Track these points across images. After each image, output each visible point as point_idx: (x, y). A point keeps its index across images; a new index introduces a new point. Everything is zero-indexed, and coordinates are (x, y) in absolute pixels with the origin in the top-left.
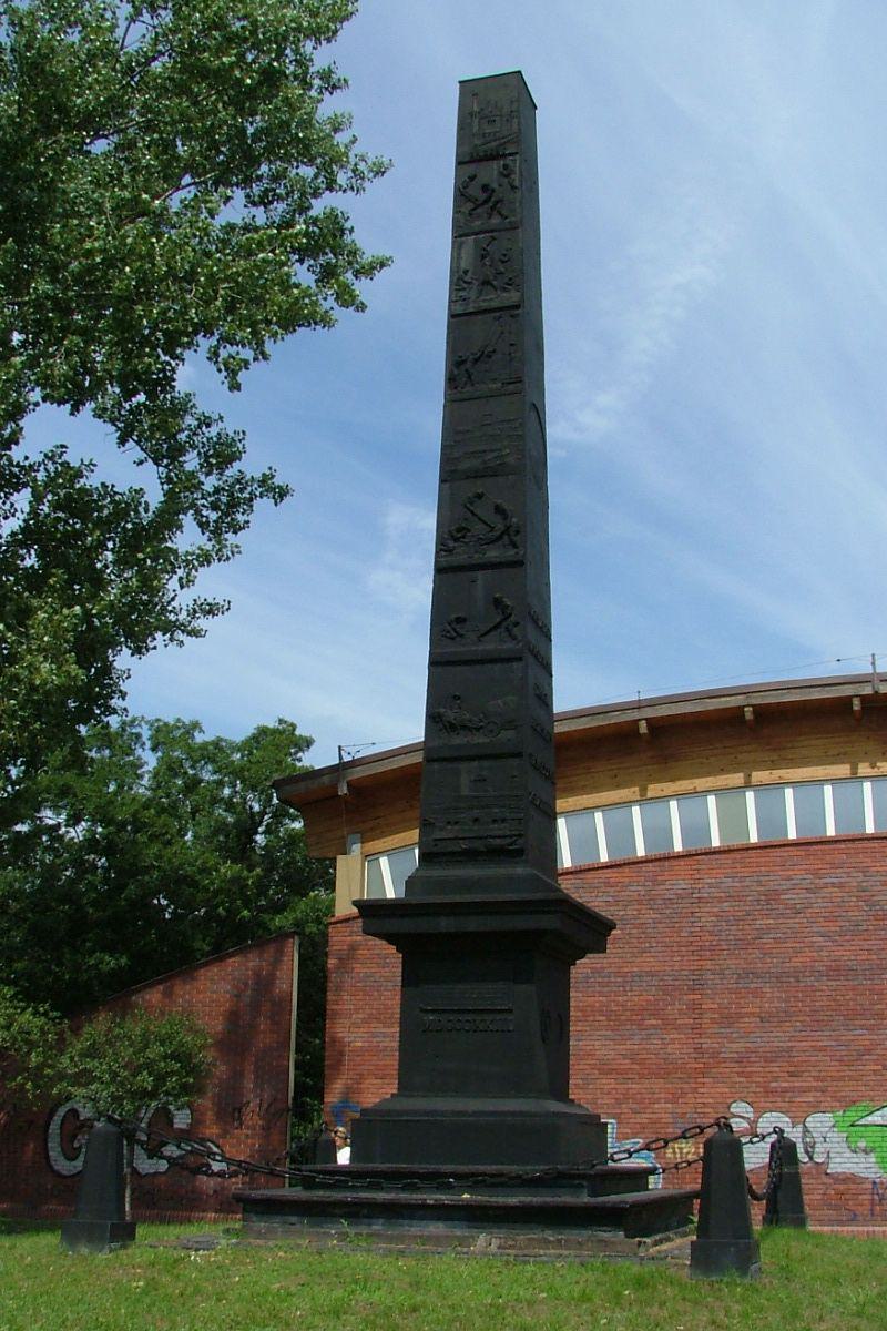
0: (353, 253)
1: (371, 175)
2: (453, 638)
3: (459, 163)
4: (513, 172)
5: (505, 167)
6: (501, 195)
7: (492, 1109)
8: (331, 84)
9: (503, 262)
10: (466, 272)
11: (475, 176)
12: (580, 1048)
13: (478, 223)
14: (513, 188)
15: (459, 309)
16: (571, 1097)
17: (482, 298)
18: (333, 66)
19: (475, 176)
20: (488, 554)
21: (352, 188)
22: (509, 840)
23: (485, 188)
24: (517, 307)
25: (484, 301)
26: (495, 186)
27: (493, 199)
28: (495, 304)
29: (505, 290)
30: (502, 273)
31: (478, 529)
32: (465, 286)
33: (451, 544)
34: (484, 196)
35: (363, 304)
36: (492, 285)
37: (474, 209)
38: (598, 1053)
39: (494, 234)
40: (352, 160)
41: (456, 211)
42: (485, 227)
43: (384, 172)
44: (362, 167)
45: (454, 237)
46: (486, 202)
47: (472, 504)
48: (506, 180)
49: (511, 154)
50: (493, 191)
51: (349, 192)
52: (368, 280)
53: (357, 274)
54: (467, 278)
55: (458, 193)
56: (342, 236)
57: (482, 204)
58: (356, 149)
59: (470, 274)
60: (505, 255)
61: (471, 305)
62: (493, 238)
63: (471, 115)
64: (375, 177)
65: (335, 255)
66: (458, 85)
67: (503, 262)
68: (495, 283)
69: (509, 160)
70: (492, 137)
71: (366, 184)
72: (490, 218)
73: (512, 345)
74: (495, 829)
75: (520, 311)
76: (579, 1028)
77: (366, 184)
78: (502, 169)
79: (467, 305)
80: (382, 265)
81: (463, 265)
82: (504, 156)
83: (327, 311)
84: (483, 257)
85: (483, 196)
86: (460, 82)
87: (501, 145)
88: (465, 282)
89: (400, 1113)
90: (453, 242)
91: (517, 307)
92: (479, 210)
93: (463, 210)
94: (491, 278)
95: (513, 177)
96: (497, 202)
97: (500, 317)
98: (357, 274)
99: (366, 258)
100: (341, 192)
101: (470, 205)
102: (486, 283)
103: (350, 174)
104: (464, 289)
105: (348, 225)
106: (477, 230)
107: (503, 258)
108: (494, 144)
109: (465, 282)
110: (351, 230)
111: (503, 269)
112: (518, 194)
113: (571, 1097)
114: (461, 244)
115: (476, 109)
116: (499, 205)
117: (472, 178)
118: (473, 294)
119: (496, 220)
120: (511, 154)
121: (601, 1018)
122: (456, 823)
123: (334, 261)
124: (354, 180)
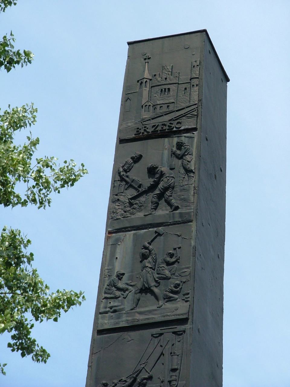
0: (35, 286)
1: (59, 183)
3: (121, 141)
4: (187, 152)
5: (180, 146)
6: (172, 181)
8: (14, 67)
9: (168, 264)
10: (120, 276)
11: (140, 157)
13: (140, 214)
14: (188, 171)
15: (107, 323)
17: (138, 310)
18: (8, 37)
19: (140, 157)
21: (34, 201)
23: (152, 171)
24: (184, 321)
25: (140, 313)
26: (165, 169)
27: (160, 186)
28: (157, 318)
29: (169, 299)
30: (167, 278)
32: (118, 293)
34: (151, 181)
35: (44, 351)
36: (153, 293)
37: (134, 198)
39: (161, 229)
40: (34, 165)
41: (114, 199)
42: (149, 220)
43: (74, 180)
44: (47, 173)
45: (109, 233)
48: (180, 161)
49: (187, 131)
50: (162, 174)
51: (29, 204)
52: (51, 321)
53: (37, 313)
54: (121, 285)
55: (118, 178)
56: (18, 264)
57: (146, 192)
58: (39, 153)
59: (125, 278)
60: (171, 256)
61: (124, 318)
62: (159, 234)
63: (141, 82)
64: (63, 186)
65: (10, 288)
66: (127, 46)
67: (168, 264)
68: (156, 290)
69: (184, 138)
70: (165, 109)
71: (52, 195)
72: (155, 209)
73: (174, 370)
75: (187, 327)
77: (52, 195)
78: (174, 149)
79: (119, 318)
80: (70, 302)
81: (118, 268)
82: (179, 132)
84: (144, 257)
85: (148, 182)
86: (129, 44)
87: (177, 118)
88: (119, 289)
90: (107, 239)
91: (184, 321)
92: (142, 199)
93: (122, 198)
94: (153, 284)
95: (188, 158)
96: (166, 189)
97: (161, 334)
98: (37, 313)
99: (50, 295)
100: (20, 205)
101: (132, 193)
102: (146, 290)
103: (32, 183)
104: (116, 298)
105: (26, 251)
106: (139, 223)
107: (168, 259)
108: (167, 118)
109: (119, 289)
110: (30, 258)
111: (167, 273)
112: (194, 180)
114: (118, 240)
115: (147, 75)
116: (168, 193)
117: (137, 159)
118: (127, 305)
119: (163, 212)
120: (187, 131)
123: (10, 296)
124: (36, 190)
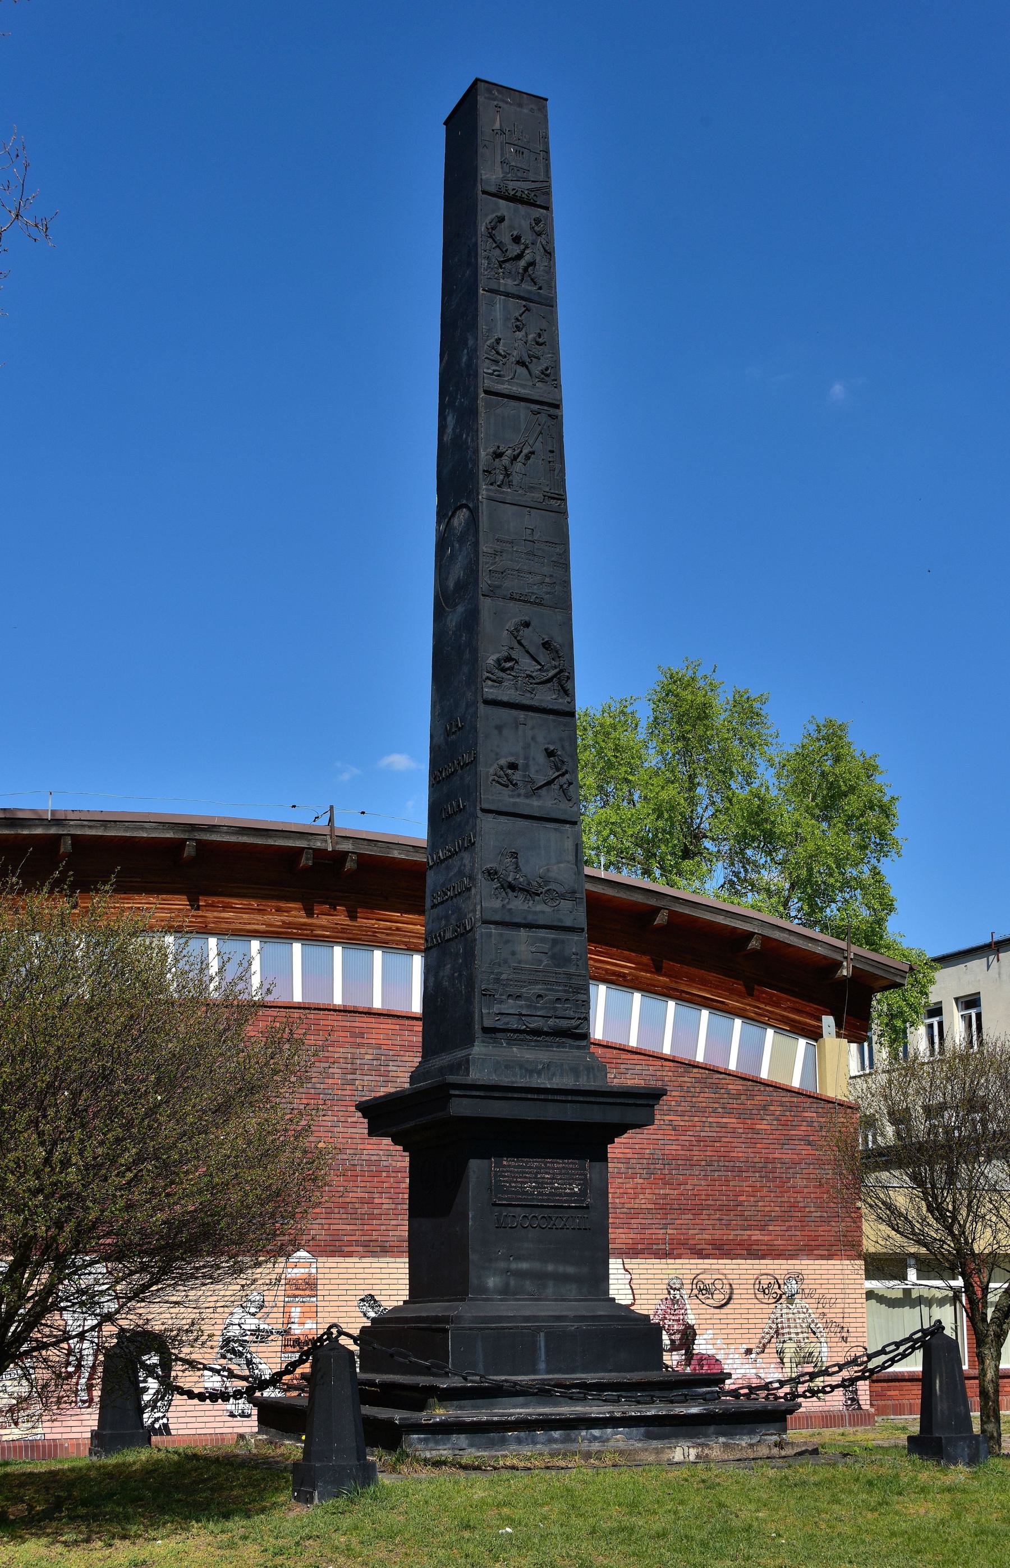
2: (507, 786)
7: (528, 1313)
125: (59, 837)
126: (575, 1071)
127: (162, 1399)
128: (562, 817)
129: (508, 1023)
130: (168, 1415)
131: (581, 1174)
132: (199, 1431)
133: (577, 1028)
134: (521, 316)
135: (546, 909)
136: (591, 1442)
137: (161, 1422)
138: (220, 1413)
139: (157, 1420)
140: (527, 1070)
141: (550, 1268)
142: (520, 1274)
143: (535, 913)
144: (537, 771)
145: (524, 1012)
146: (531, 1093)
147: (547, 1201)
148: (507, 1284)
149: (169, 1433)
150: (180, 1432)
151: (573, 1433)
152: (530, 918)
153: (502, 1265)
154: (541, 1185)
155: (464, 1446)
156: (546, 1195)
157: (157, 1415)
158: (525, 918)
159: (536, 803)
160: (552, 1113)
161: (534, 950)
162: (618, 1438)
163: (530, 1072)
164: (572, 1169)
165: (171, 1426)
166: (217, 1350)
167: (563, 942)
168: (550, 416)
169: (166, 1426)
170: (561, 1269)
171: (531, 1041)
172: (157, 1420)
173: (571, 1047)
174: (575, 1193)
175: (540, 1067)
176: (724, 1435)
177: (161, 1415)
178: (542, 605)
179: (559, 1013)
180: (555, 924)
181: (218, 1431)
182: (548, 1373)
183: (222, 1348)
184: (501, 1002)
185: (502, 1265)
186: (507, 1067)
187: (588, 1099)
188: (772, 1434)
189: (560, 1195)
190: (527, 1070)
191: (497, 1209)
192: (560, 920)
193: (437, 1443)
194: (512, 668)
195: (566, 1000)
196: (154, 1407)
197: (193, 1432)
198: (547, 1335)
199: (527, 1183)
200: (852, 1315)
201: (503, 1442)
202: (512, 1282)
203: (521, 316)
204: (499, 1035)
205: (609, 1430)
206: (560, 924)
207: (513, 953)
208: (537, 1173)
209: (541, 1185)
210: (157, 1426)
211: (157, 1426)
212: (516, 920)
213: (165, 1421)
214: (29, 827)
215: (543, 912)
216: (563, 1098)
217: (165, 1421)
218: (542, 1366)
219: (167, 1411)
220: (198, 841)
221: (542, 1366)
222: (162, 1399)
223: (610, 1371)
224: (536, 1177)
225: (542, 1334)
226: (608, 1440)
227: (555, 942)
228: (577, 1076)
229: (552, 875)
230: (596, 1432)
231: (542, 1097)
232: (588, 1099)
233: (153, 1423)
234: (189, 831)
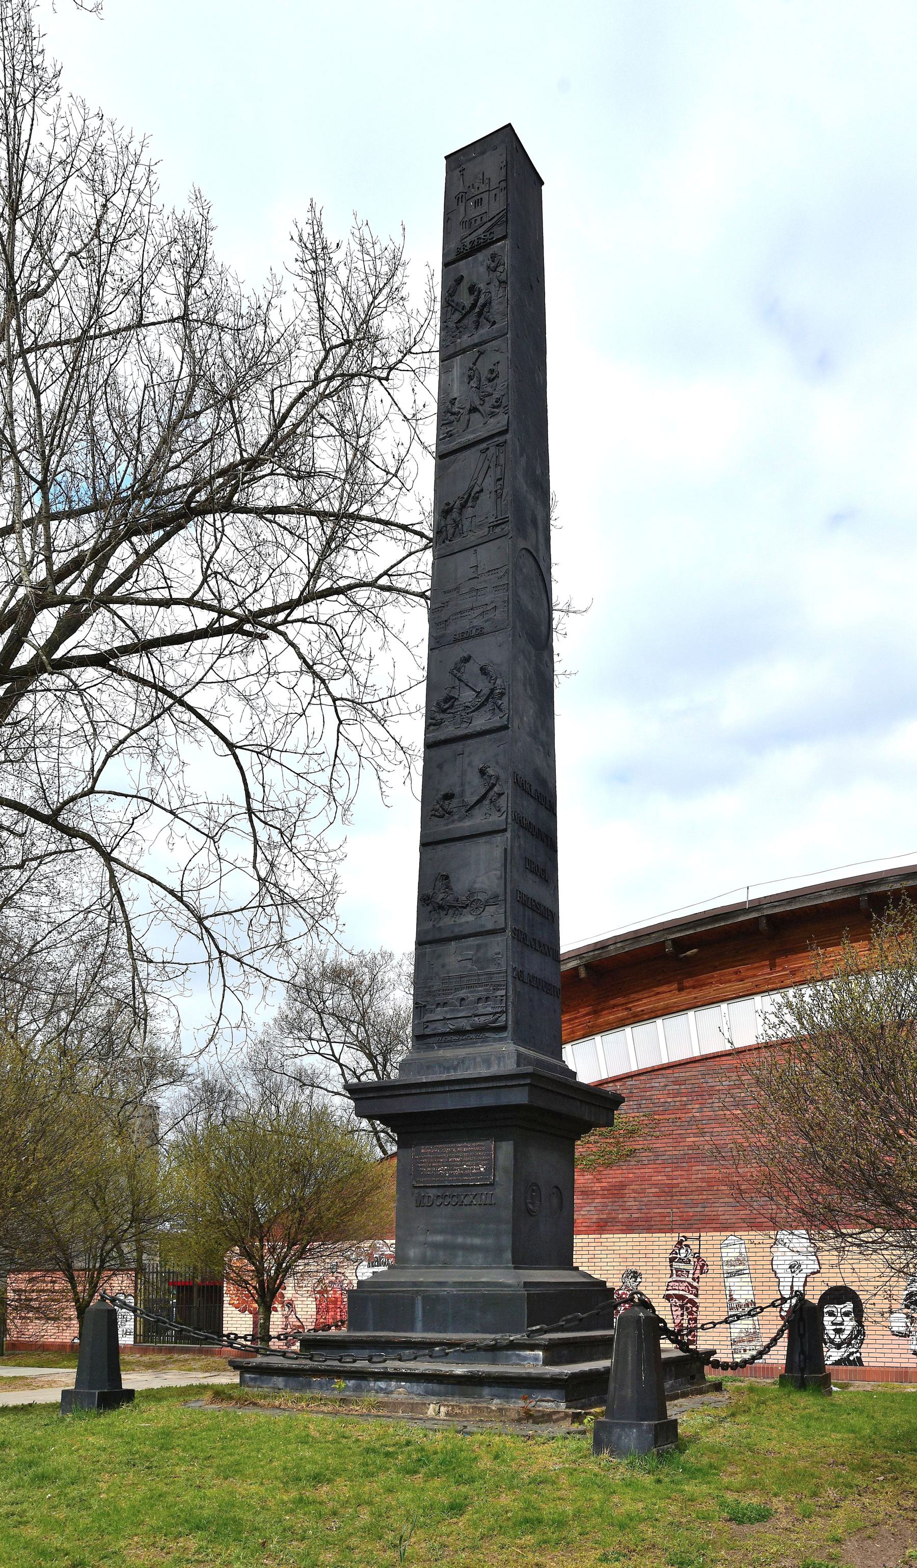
2: (442, 817)
5: (493, 257)
7: (471, 1280)
12: (705, 1213)
16: (575, 1265)
20: (474, 723)
22: (491, 1018)
31: (467, 696)
33: (439, 716)
38: (721, 1217)
46: (474, 306)
47: (459, 670)
62: (481, 353)
74: (482, 1008)
76: (704, 1197)
83: (870, 939)
84: (471, 378)
89: (393, 1284)
113: (575, 1265)
121: (723, 1188)
122: (445, 1004)
125: (756, 919)
126: (487, 1062)
127: (856, 1338)
128: (490, 829)
129: (435, 1029)
130: (861, 1350)
131: (487, 1155)
132: (887, 1365)
133: (495, 1021)
134: (474, 364)
135: (470, 918)
136: (377, 1393)
137: (855, 1355)
138: (905, 1351)
139: (852, 1353)
140: (444, 1067)
141: (460, 1240)
142: (435, 1246)
143: (461, 925)
144: (472, 794)
145: (448, 1016)
146: (416, 1088)
147: (458, 1180)
148: (424, 1256)
149: (861, 1364)
150: (871, 1364)
151: (364, 1383)
152: (457, 931)
153: (421, 1238)
154: (451, 1167)
155: (281, 1386)
156: (456, 1176)
157: (851, 1350)
158: (453, 932)
159: (467, 823)
160: (472, 1101)
161: (460, 959)
162: (401, 1391)
163: (448, 1069)
164: (479, 1151)
165: (863, 1359)
166: (902, 1301)
167: (486, 945)
168: (497, 445)
169: (859, 1359)
170: (469, 1241)
171: (458, 1040)
172: (852, 1353)
173: (495, 1040)
174: (481, 1172)
175: (456, 1063)
176: (499, 1397)
177: (855, 1350)
178: (483, 634)
179: (479, 1012)
180: (478, 930)
181: (903, 1365)
182: (424, 1331)
183: (905, 1300)
184: (432, 1011)
185: (421, 1238)
186: (428, 1067)
187: (491, 1085)
188: (548, 1401)
189: (467, 1175)
190: (444, 1067)
191: (416, 1191)
192: (483, 926)
193: (262, 1381)
194: (452, 707)
195: (487, 998)
196: (849, 1344)
197: (882, 1364)
198: (424, 1298)
199: (440, 1166)
200: (757, 1280)
201: (309, 1385)
202: (429, 1253)
203: (474, 364)
204: (430, 1040)
205: (393, 1383)
206: (483, 929)
207: (443, 966)
208: (450, 1157)
209: (451, 1167)
210: (851, 1358)
211: (851, 1358)
212: (444, 936)
213: (858, 1355)
214: (739, 915)
215: (467, 922)
216: (441, 1089)
217: (858, 1355)
218: (419, 1325)
219: (860, 1347)
220: (869, 895)
221: (419, 1325)
222: (856, 1338)
223: (477, 1332)
224: (448, 1161)
225: (420, 1298)
226: (392, 1392)
227: (479, 947)
228: (489, 1067)
229: (477, 886)
230: (382, 1384)
231: (424, 1090)
232: (491, 1085)
233: (849, 1356)
234: (860, 889)
